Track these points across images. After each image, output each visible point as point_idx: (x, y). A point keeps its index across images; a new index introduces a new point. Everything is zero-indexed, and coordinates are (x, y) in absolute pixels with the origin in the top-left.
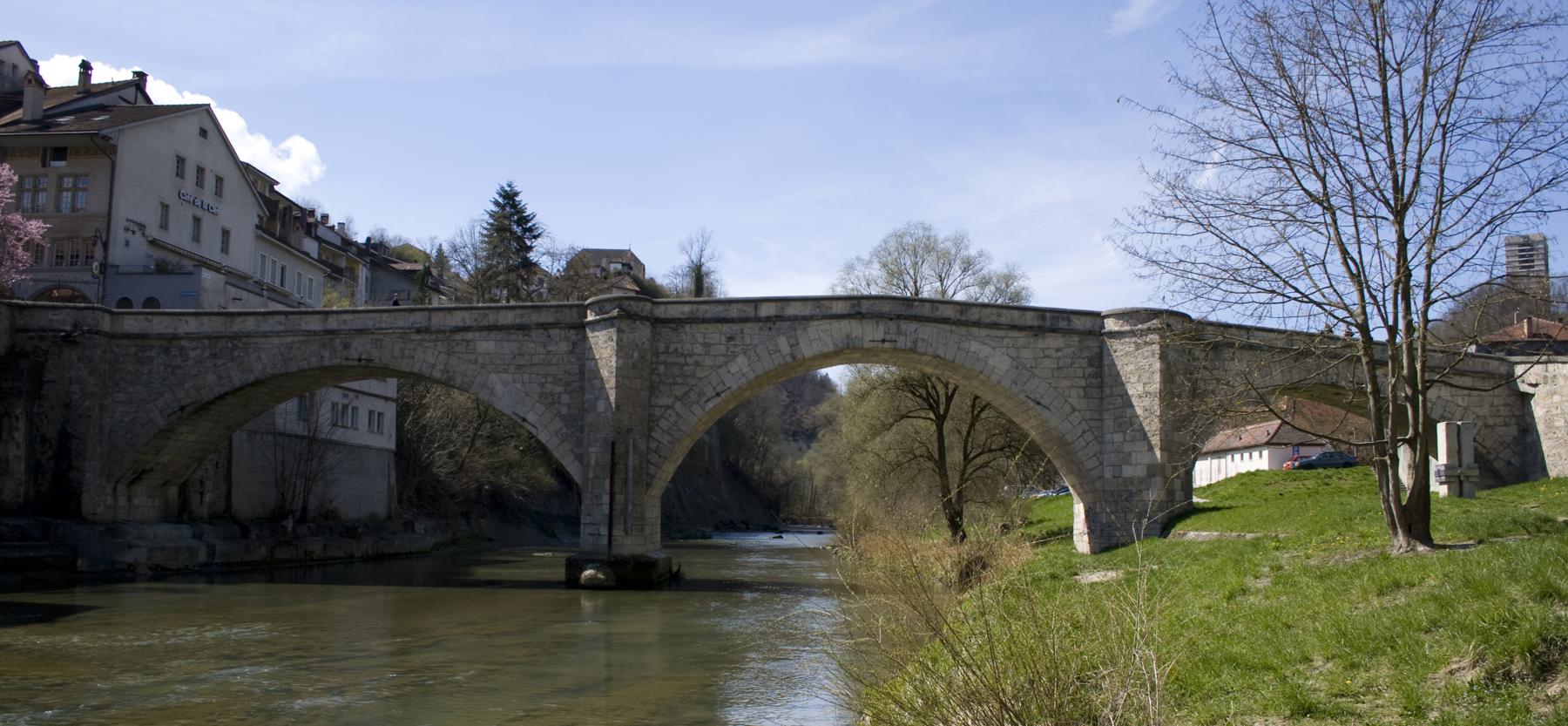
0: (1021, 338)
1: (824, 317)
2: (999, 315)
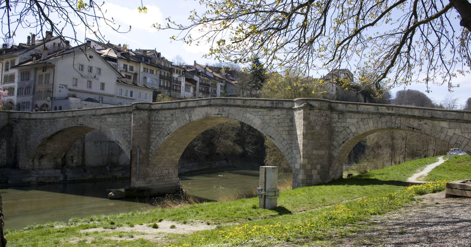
0: (265, 111)
1: (199, 107)
2: (257, 103)
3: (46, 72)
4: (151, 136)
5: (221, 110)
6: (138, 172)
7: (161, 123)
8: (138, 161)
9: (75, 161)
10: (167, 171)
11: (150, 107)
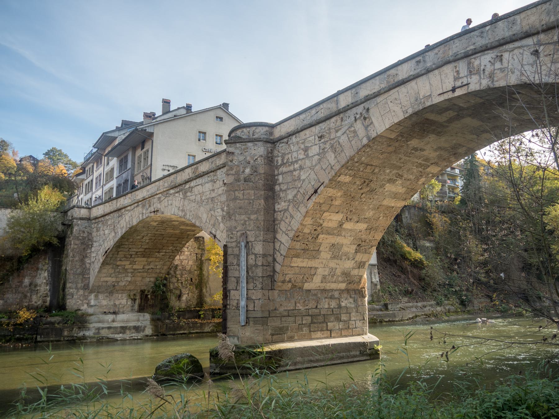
3: (145, 150)
4: (277, 207)
5: (464, 71)
6: (243, 303)
7: (297, 166)
8: (244, 273)
9: (184, 298)
10: (333, 304)
11: (271, 134)
